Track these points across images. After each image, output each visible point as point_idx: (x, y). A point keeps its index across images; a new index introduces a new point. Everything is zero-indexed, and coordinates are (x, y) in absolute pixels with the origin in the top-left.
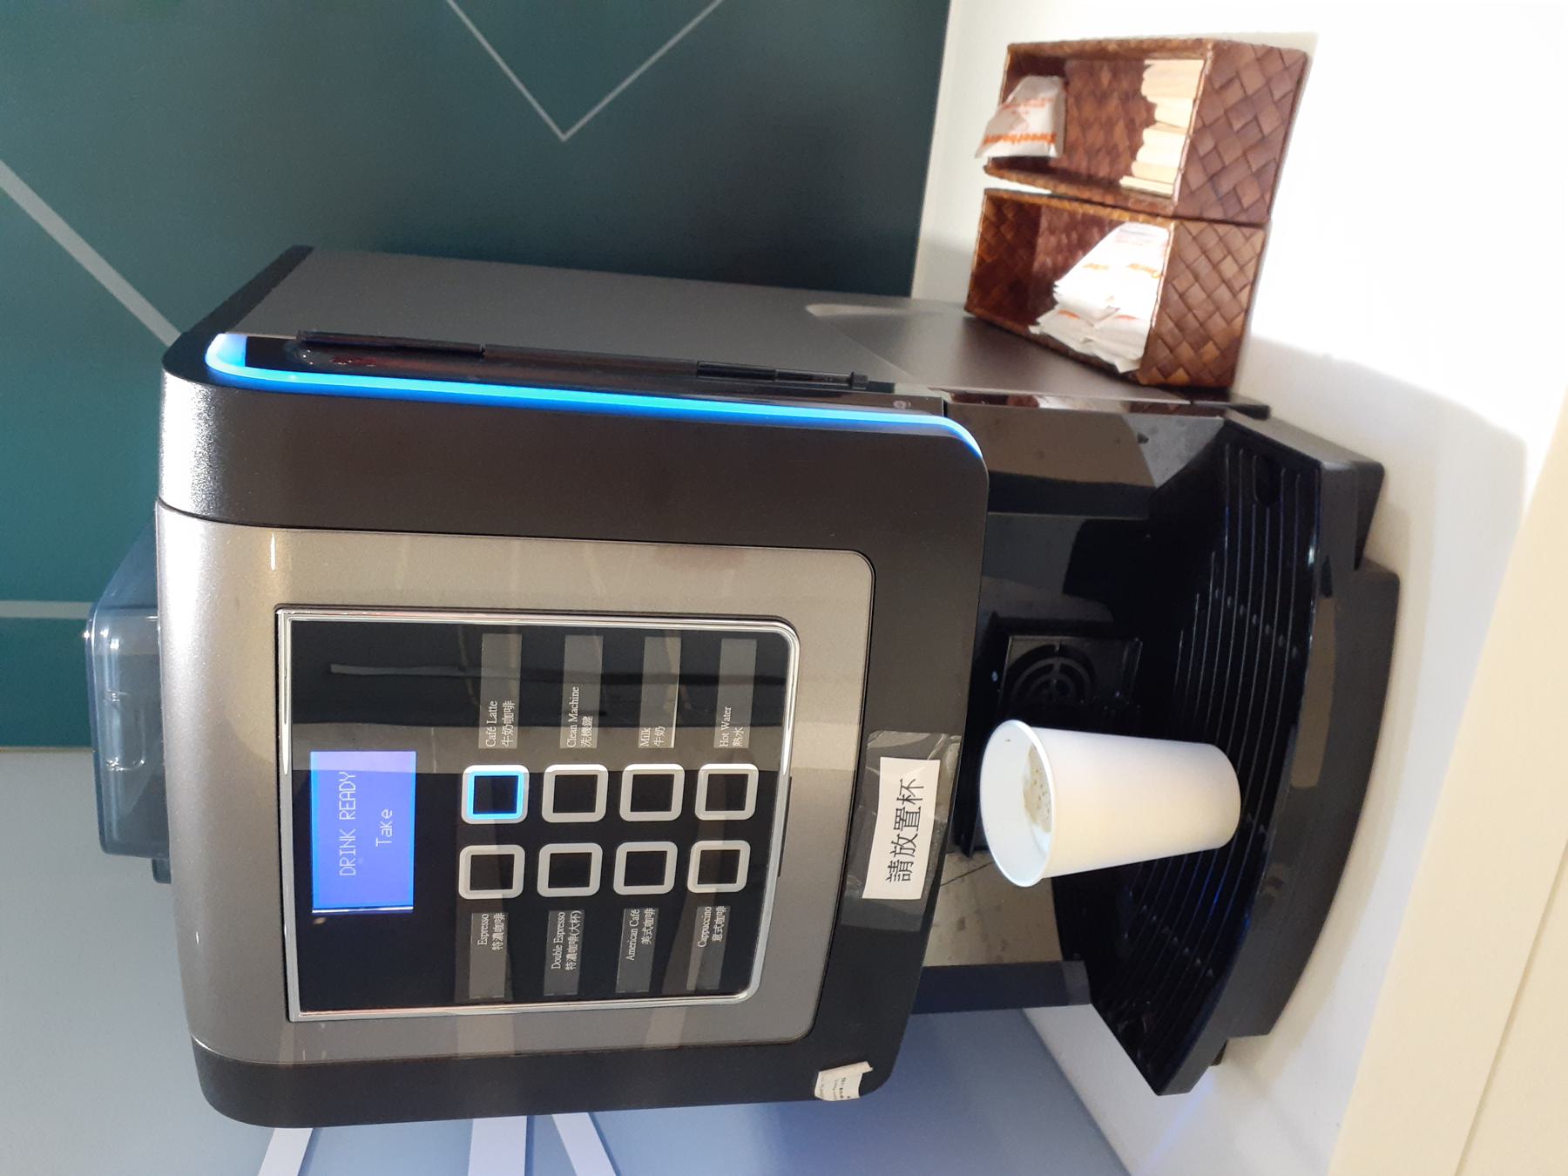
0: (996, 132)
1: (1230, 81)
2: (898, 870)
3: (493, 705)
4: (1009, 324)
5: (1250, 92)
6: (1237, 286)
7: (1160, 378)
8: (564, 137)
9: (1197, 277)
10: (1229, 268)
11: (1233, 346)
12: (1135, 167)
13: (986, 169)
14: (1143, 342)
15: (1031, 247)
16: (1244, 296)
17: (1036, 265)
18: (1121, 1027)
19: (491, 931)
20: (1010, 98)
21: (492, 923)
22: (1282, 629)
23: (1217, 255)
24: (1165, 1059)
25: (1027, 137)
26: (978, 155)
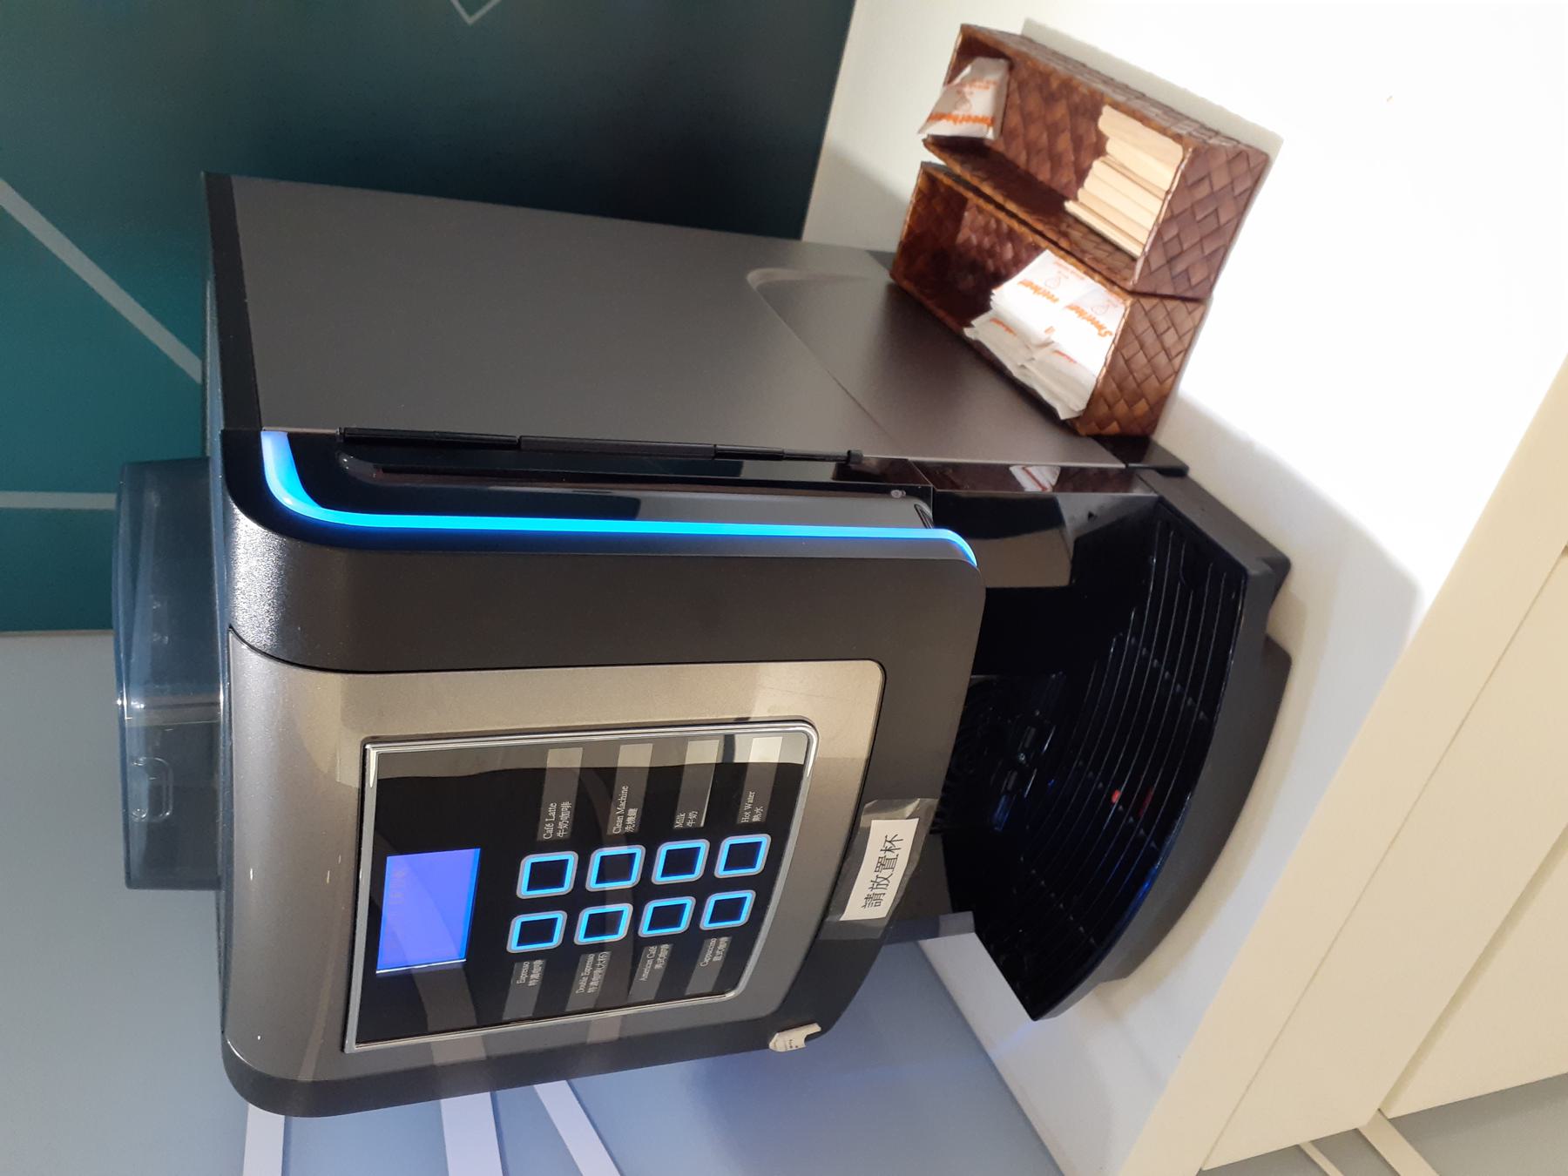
0: (945, 111)
1: (1201, 180)
2: (872, 900)
3: (553, 806)
4: (941, 313)
5: (1216, 188)
6: (1173, 353)
7: (1096, 430)
8: (470, 20)
9: (1142, 347)
10: (1170, 338)
11: (1161, 400)
12: (1080, 193)
13: (924, 141)
14: (1087, 397)
15: (958, 219)
16: (1177, 361)
17: (961, 238)
18: (1003, 958)
19: (529, 973)
20: (958, 80)
21: (531, 967)
22: (1194, 693)
23: (1162, 327)
24: (1042, 990)
25: (968, 119)
26: (921, 131)
